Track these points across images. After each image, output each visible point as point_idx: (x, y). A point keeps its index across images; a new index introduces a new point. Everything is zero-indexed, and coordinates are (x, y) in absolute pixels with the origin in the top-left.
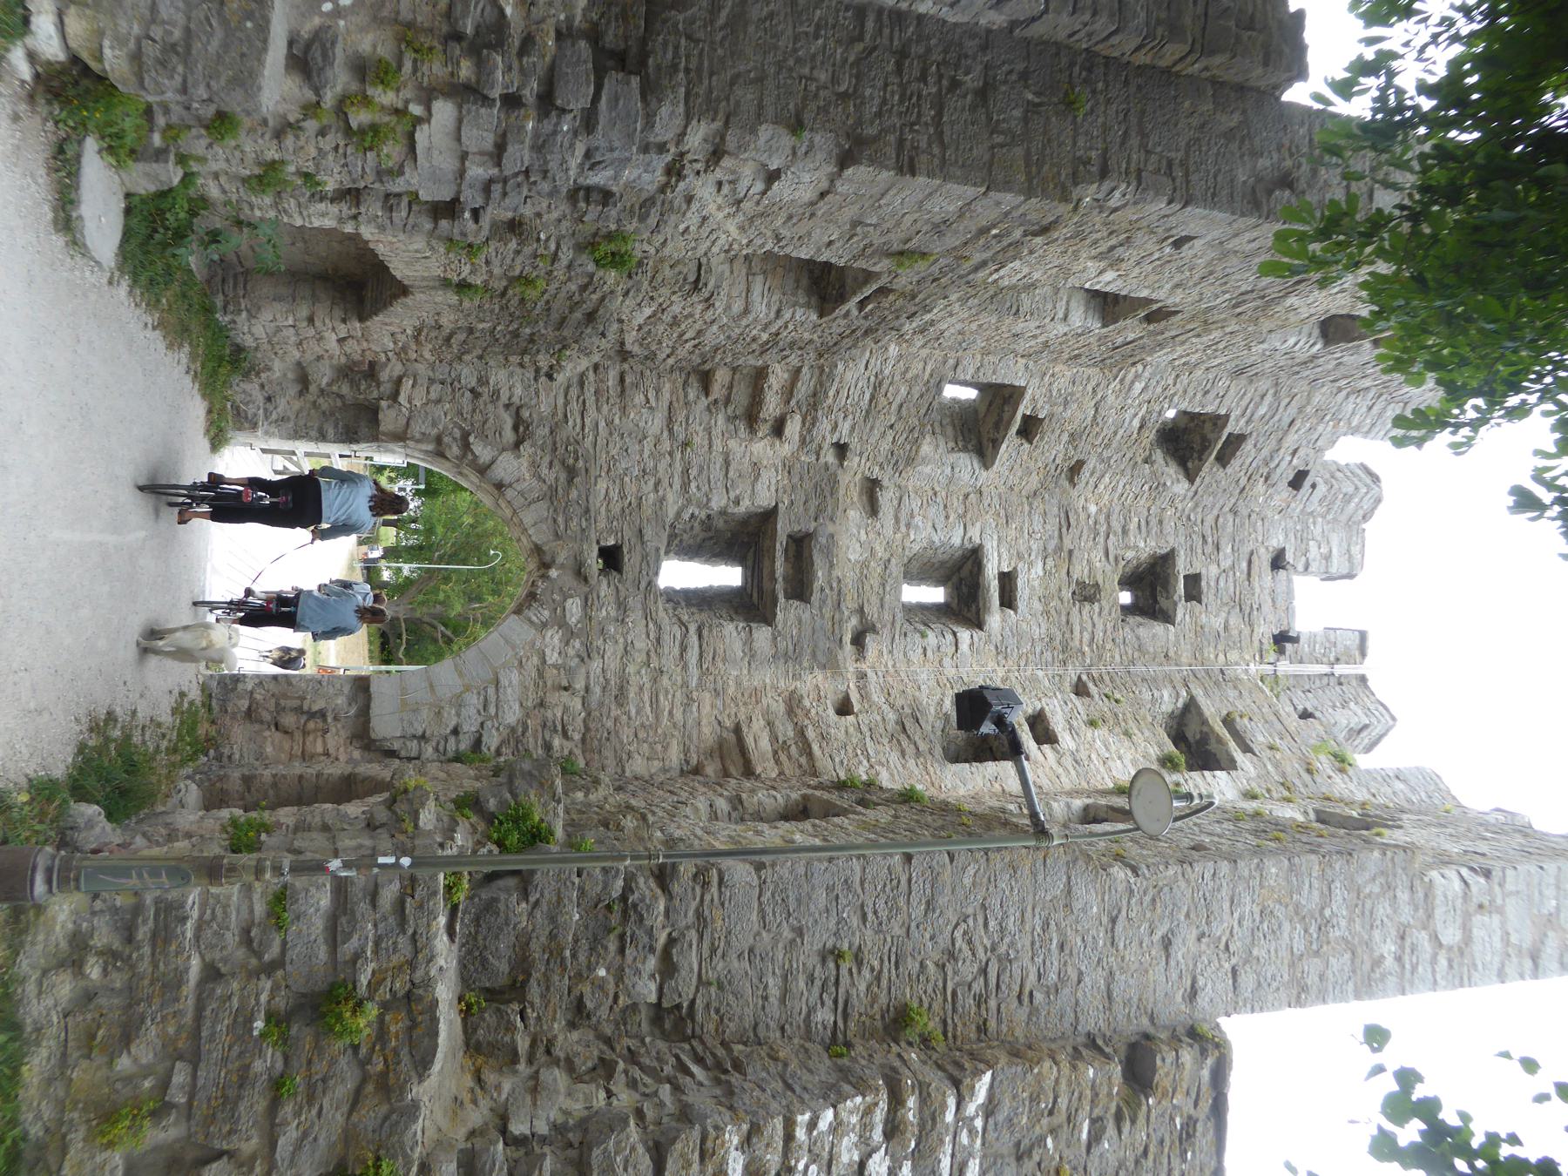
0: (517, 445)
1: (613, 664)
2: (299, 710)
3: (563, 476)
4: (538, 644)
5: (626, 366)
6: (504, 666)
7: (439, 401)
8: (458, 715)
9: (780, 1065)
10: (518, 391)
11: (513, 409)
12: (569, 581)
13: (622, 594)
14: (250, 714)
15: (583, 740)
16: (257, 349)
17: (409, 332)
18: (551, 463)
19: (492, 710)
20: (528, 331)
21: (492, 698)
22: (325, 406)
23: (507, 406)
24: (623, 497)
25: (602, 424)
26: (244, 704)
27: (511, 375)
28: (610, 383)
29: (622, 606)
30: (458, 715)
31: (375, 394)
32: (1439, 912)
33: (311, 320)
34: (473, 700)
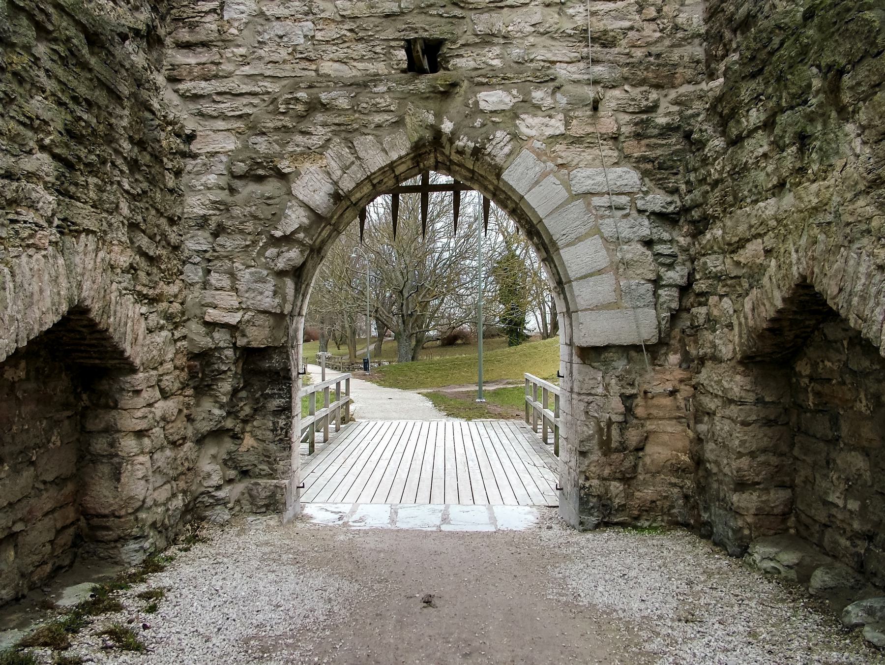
0: (282, 176)
1: (561, 51)
2: (623, 426)
3: (320, 117)
4: (538, 144)
5: (168, 41)
6: (568, 187)
7: (232, 275)
8: (628, 241)
9: (719, 109)
10: (212, 179)
11: (237, 184)
12: (456, 104)
13: (472, 39)
14: (627, 478)
15: (658, 86)
16: (184, 492)
17: (144, 310)
18: (304, 133)
19: (624, 200)
20: (126, 145)
21: (604, 201)
22: (247, 410)
23: (232, 191)
24: (343, 40)
25: (247, 70)
26: (616, 487)
27: (192, 188)
28: (193, 61)
29: (486, 39)
30: (628, 241)
31: (229, 353)
32: (276, 345)
33: (140, 434)
34: (608, 227)
